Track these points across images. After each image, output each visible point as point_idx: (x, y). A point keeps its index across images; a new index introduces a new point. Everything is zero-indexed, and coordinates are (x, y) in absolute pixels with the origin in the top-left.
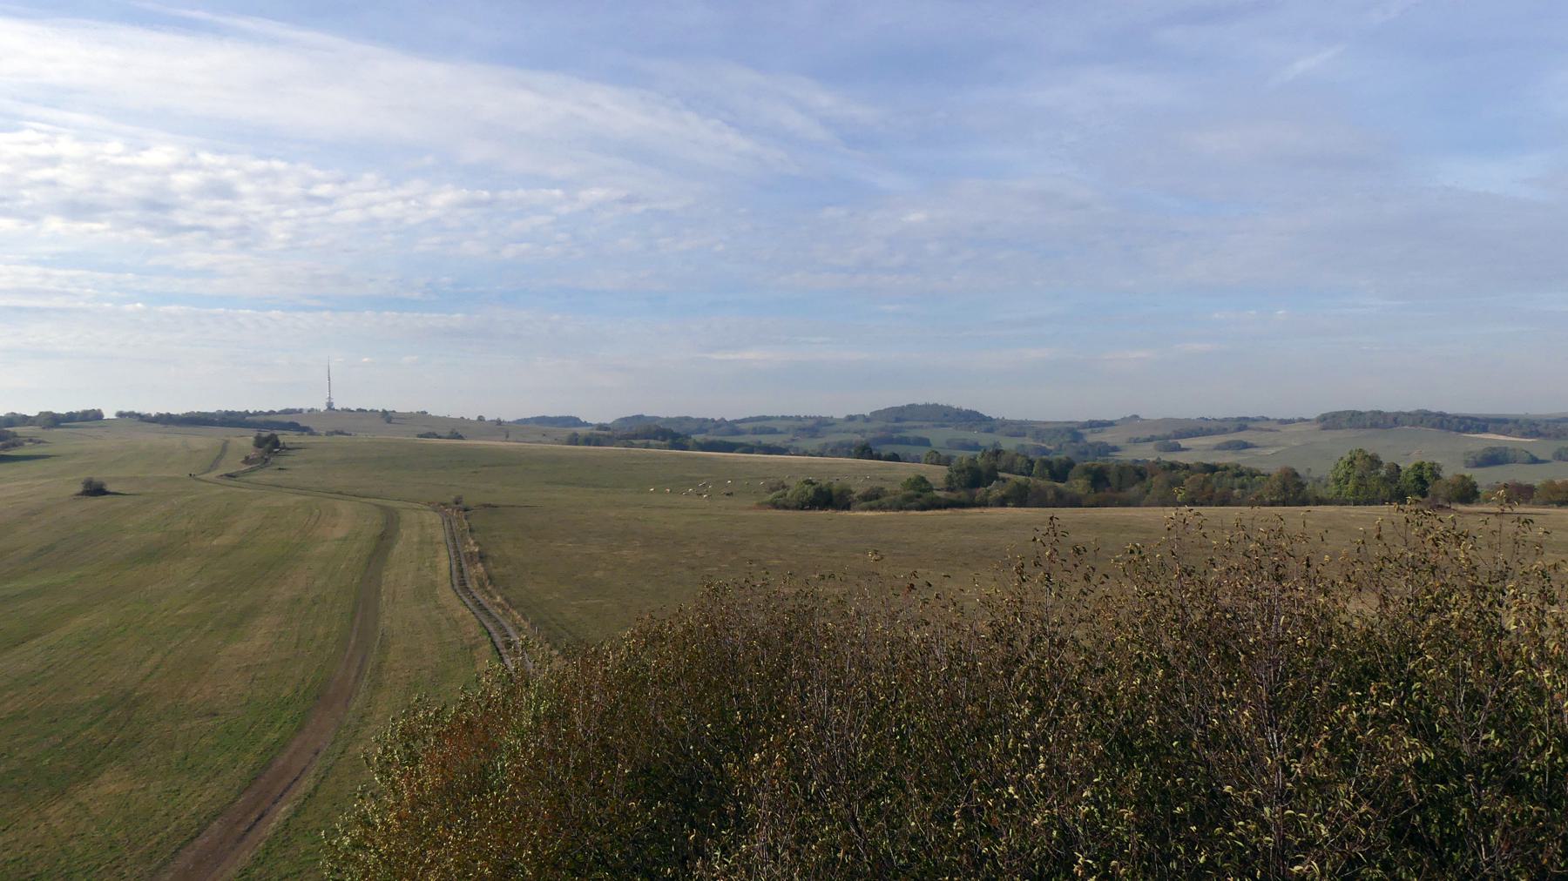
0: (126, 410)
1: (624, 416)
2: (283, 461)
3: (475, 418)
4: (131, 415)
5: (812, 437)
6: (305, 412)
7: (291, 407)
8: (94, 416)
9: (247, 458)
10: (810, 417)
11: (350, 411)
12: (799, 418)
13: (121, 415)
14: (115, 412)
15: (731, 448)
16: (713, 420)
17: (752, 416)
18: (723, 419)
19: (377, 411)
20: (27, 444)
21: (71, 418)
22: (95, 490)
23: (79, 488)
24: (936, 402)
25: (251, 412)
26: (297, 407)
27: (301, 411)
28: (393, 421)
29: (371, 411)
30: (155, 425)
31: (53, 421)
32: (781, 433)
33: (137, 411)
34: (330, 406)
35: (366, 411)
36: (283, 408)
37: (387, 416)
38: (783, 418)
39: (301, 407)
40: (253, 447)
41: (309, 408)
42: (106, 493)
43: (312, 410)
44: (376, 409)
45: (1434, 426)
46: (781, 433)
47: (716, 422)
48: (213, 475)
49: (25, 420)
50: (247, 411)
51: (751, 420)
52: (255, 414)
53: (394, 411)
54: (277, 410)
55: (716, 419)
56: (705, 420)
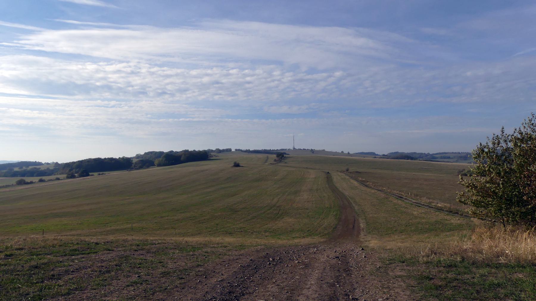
0: (238, 149)
1: (391, 152)
2: (286, 161)
3: (341, 152)
4: (239, 150)
5: (465, 160)
6: (287, 150)
7: (267, 149)
8: (230, 150)
9: (275, 160)
10: (464, 153)
11: (301, 149)
12: (459, 153)
13: (236, 150)
14: (235, 149)
15: (449, 162)
16: (425, 154)
17: (440, 152)
18: (429, 153)
19: (309, 149)
20: (214, 157)
21: (223, 151)
22: (237, 165)
23: (233, 165)
24: (89, 158)
25: (272, 150)
26: (285, 148)
27: (286, 149)
28: (314, 153)
29: (308, 149)
30: (246, 153)
31: (219, 151)
32: (452, 158)
33: (240, 149)
34: (294, 148)
35: (306, 149)
36: (281, 149)
37: (312, 151)
38: (452, 153)
39: (286, 148)
40: (276, 157)
41: (288, 148)
42: (239, 166)
43: (289, 149)
44: (309, 149)
45: (339, 172)
46: (452, 158)
47: (466, 153)
48: (267, 164)
49: (212, 151)
50: (270, 149)
51: (440, 153)
52: (273, 150)
53: (314, 150)
54: (279, 149)
55: (426, 153)
56: (422, 154)
